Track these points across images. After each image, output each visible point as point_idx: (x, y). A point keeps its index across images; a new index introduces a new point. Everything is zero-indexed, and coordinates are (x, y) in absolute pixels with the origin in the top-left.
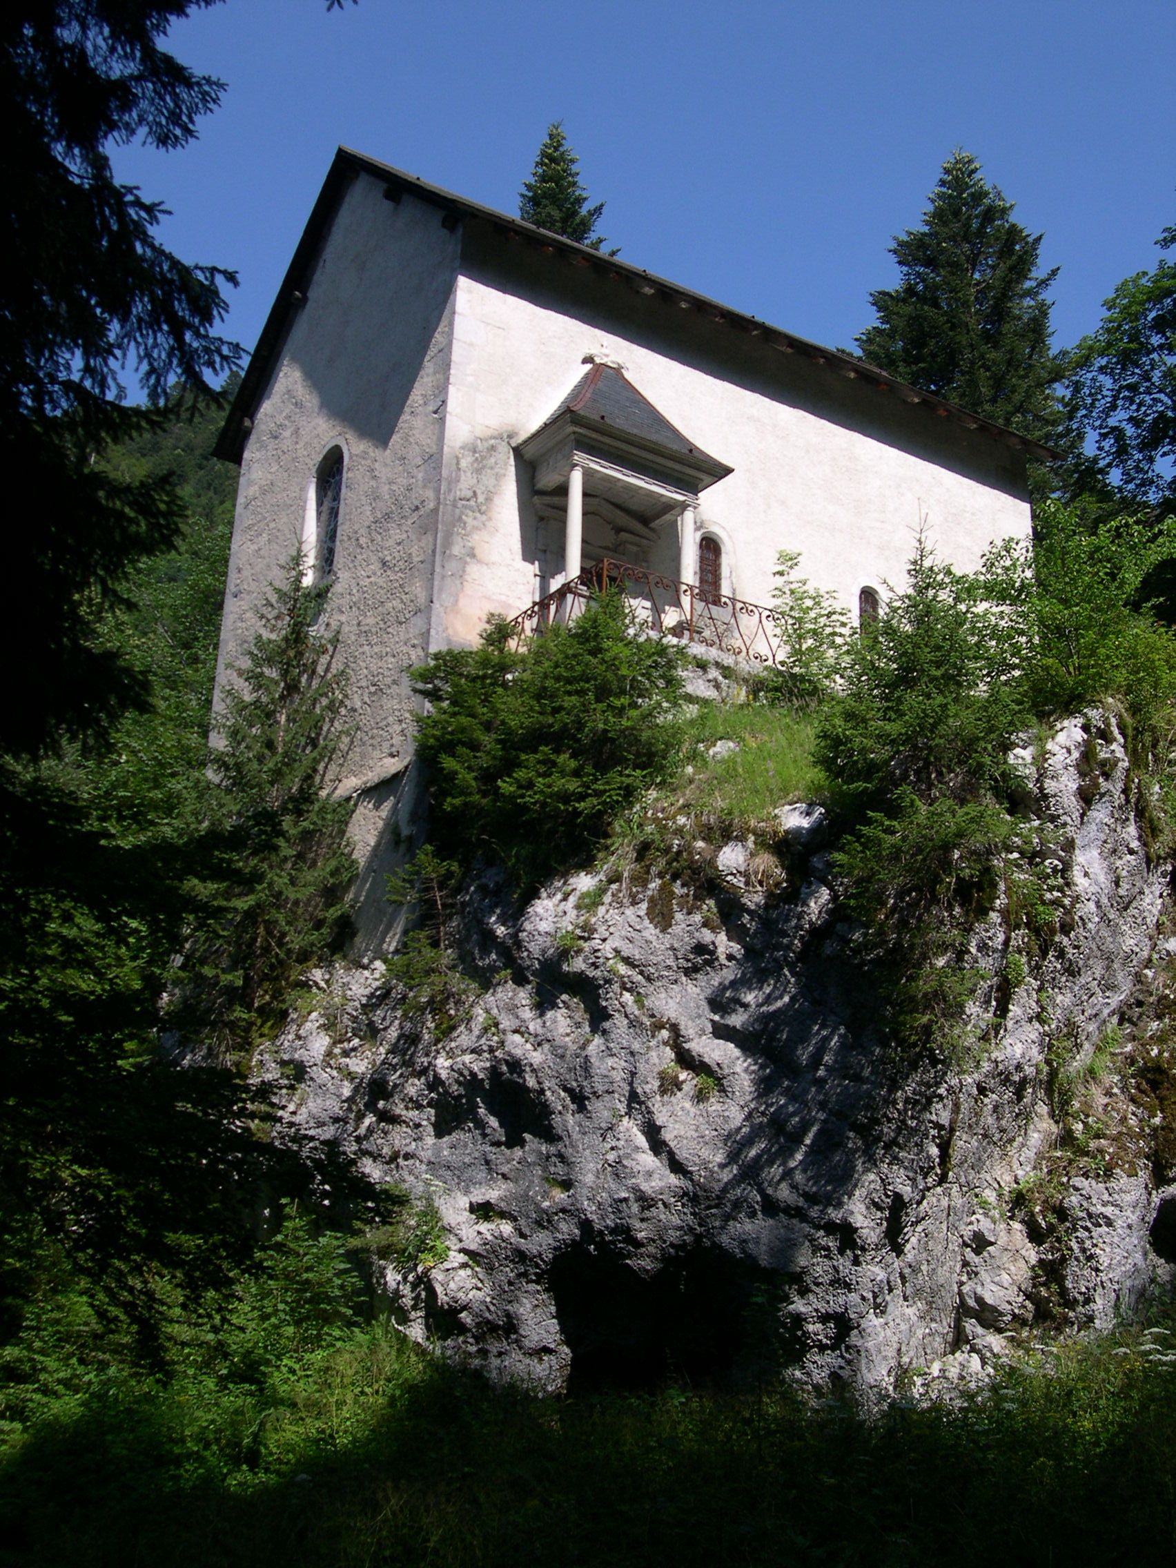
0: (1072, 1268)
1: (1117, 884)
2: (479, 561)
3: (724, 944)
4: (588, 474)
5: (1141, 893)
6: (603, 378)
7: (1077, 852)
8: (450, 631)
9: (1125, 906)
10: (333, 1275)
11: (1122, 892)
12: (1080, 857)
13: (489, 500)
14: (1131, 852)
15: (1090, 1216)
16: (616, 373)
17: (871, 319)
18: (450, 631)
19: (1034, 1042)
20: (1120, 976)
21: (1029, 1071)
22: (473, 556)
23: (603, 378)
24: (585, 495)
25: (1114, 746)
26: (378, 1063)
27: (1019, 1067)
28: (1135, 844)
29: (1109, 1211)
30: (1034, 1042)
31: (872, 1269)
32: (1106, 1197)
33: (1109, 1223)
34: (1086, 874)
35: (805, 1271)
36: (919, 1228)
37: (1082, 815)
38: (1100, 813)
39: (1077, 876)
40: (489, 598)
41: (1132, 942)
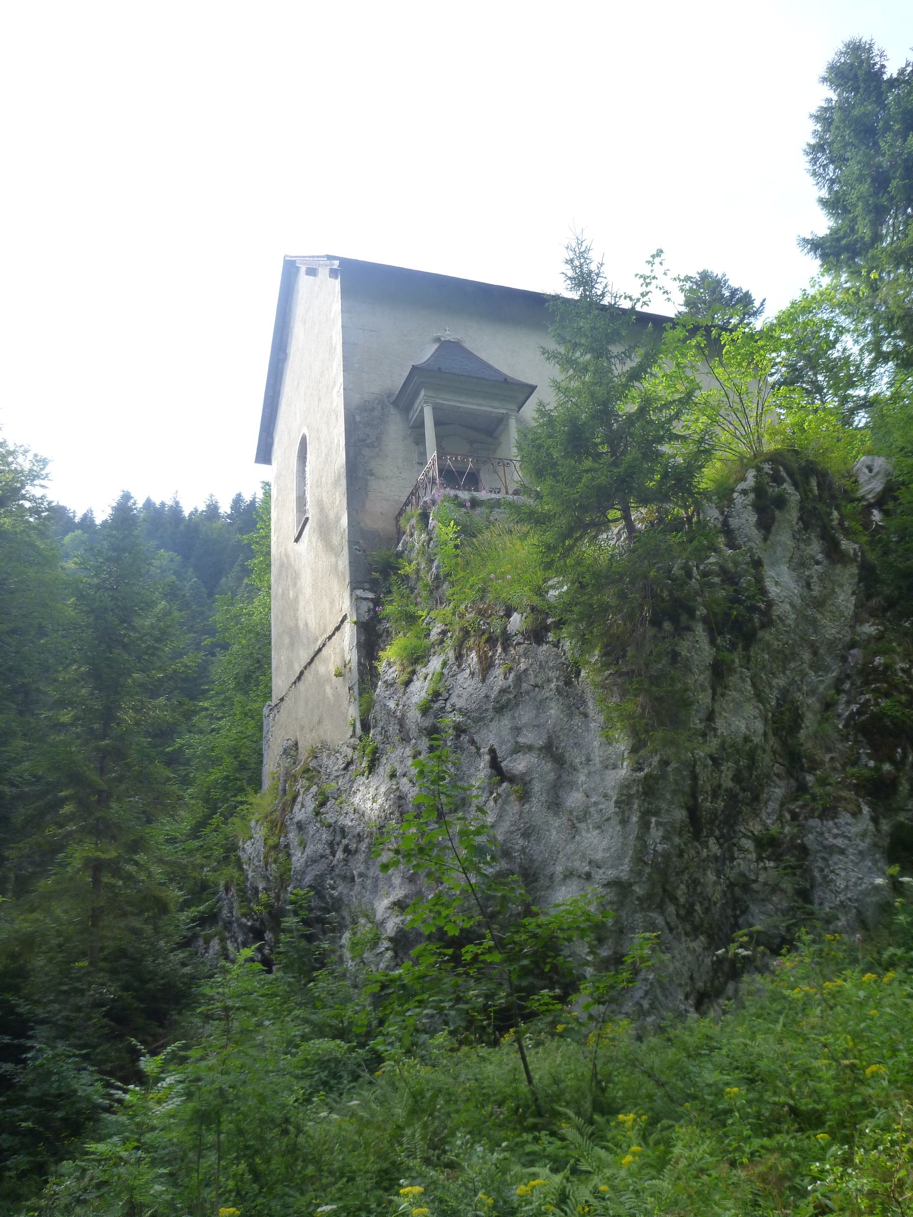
0: (818, 893)
1: (808, 585)
5: (833, 592)
6: (450, 348)
8: (362, 524)
12: (769, 573)
13: (379, 439)
14: (818, 563)
16: (456, 346)
17: (828, 232)
18: (362, 524)
19: (755, 718)
21: (757, 740)
22: (373, 475)
23: (448, 348)
26: (820, 1074)
27: (746, 739)
28: (820, 557)
29: (839, 842)
31: (652, 914)
32: (835, 831)
33: (842, 852)
34: (777, 583)
36: (686, 877)
38: (784, 537)
39: (769, 585)
41: (833, 631)
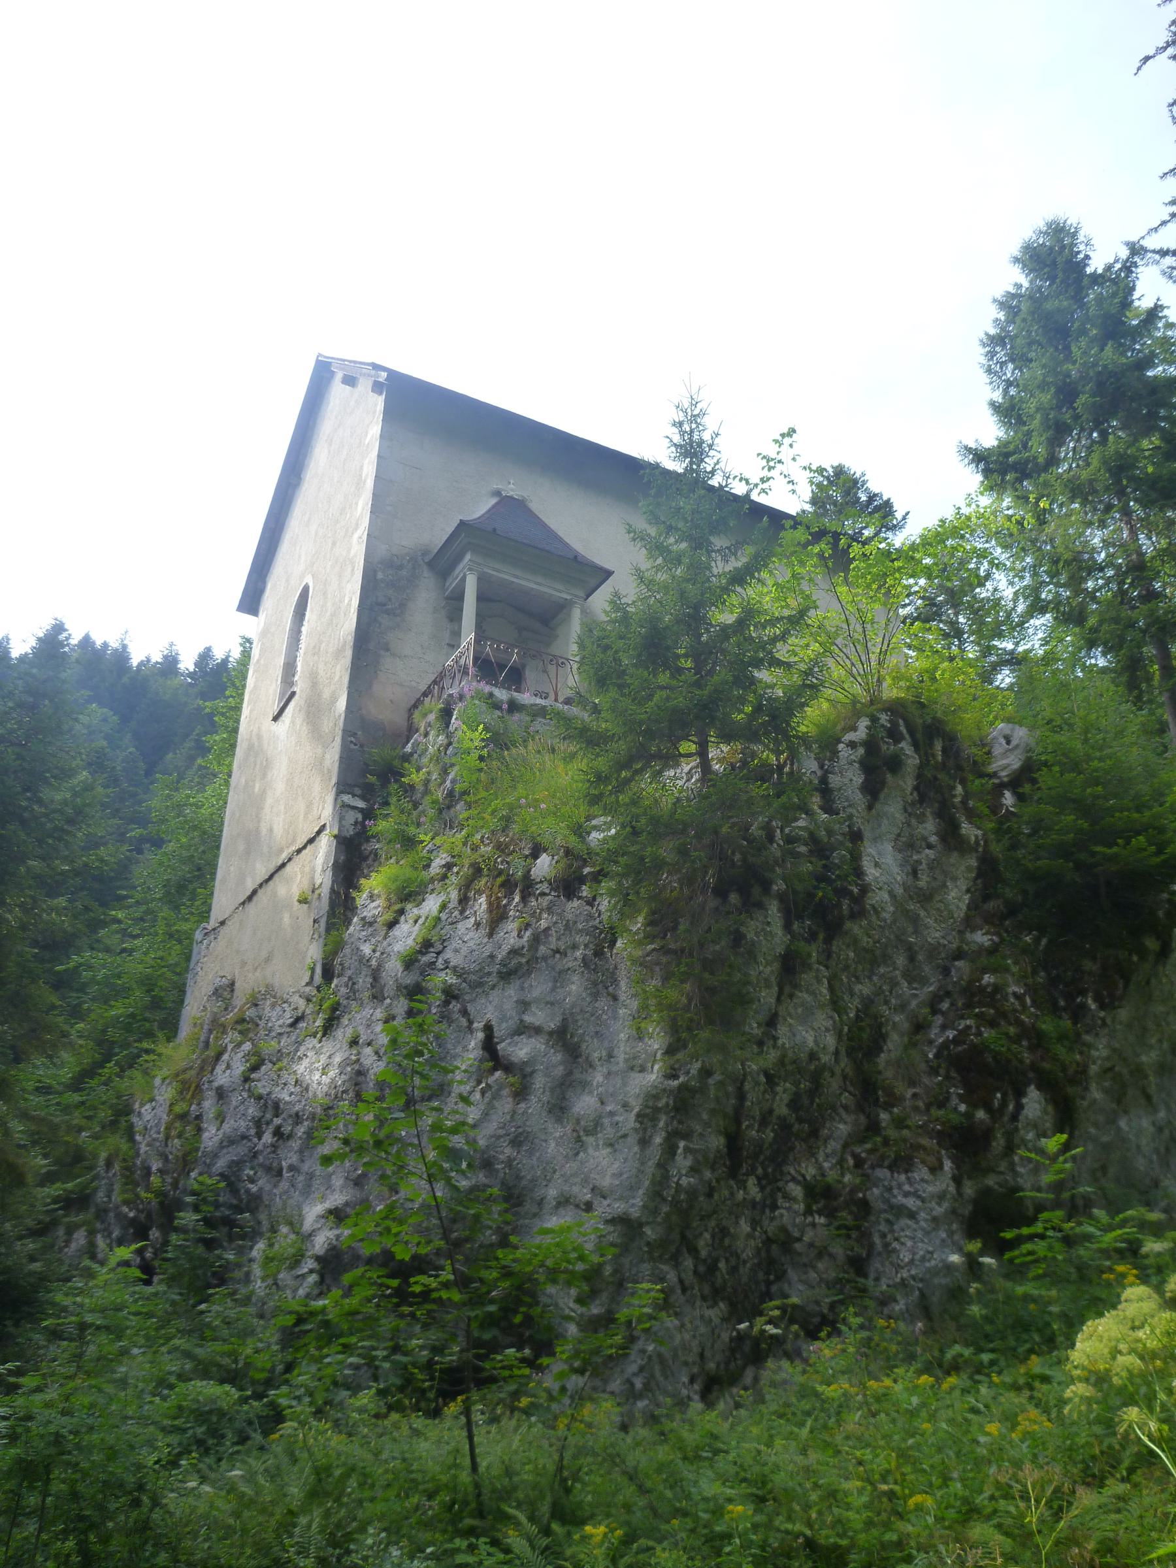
1: (915, 873)
2: (394, 655)
3: (1016, 1158)
4: (482, 580)
5: (944, 886)
7: (866, 843)
9: (926, 898)
10: (204, 1208)
11: (922, 884)
12: (869, 850)
14: (930, 846)
15: (892, 1207)
19: (827, 1030)
20: (927, 969)
21: (825, 1058)
22: (387, 650)
23: (509, 505)
24: (481, 598)
25: (903, 744)
27: (813, 1056)
29: (910, 1202)
30: (827, 1030)
32: (907, 1188)
33: (912, 1215)
35: (715, 1304)
37: (870, 808)
38: (893, 809)
40: (401, 685)
41: (937, 935)
